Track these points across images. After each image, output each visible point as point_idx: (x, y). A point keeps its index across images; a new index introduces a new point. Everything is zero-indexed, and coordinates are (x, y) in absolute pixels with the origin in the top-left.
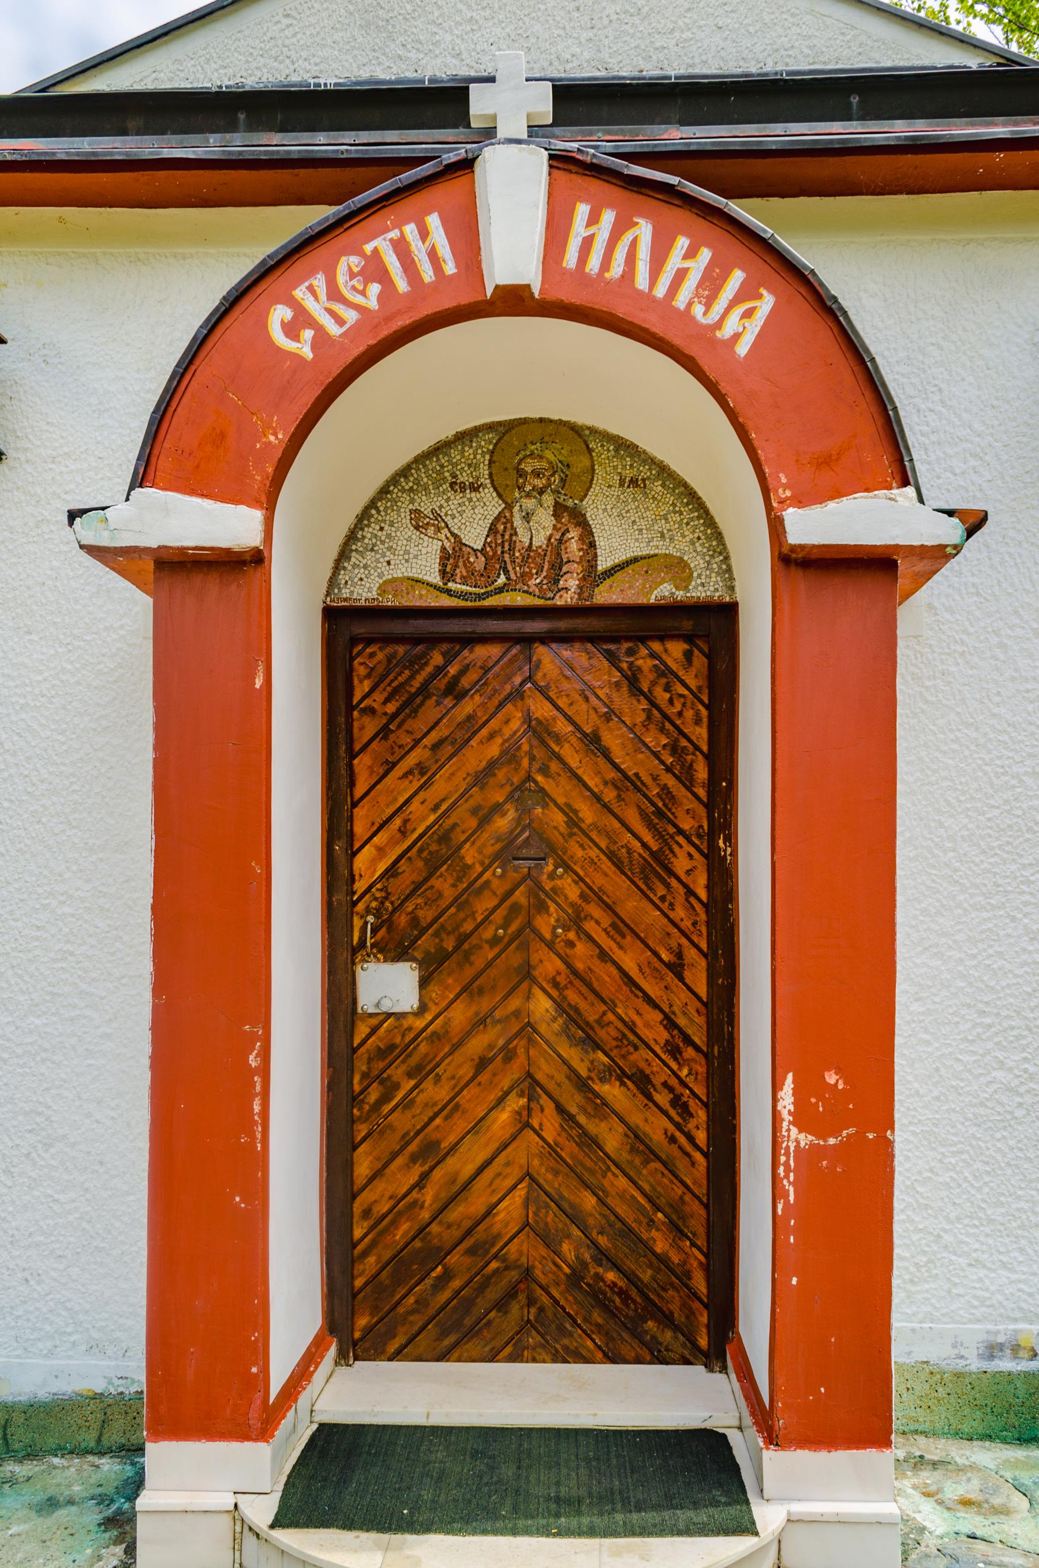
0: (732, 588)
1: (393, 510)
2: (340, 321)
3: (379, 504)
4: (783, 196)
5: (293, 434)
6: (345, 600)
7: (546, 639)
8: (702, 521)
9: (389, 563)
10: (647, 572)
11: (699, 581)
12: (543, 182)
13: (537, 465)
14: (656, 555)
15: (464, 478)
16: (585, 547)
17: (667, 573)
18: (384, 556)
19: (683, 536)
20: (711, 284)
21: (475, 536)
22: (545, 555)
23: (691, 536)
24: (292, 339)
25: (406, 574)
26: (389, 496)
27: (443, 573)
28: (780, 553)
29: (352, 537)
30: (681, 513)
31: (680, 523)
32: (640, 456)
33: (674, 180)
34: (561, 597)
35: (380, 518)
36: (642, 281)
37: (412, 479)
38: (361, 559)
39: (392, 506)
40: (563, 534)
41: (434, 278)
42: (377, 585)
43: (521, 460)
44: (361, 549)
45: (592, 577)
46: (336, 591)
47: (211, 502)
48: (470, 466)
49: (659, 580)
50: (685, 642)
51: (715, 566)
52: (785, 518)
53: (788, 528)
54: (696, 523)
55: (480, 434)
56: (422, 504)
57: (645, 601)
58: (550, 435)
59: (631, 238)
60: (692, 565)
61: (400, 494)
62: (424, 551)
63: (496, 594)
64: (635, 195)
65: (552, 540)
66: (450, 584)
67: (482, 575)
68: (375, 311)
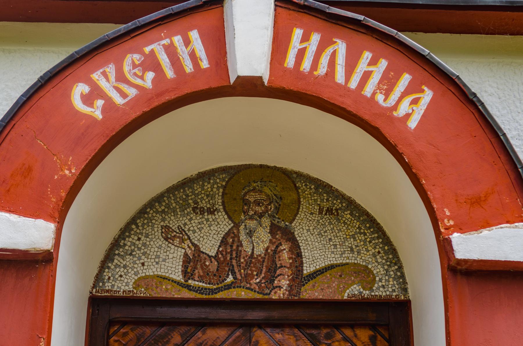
0: (405, 290)
1: (148, 226)
2: (124, 95)
3: (138, 221)
4: (426, 32)
5: (83, 170)
6: (108, 291)
7: (262, 325)
8: (381, 240)
9: (143, 264)
10: (341, 276)
11: (380, 284)
12: (271, 14)
13: (258, 197)
14: (347, 264)
15: (203, 204)
16: (294, 256)
17: (356, 277)
18: (139, 259)
19: (368, 251)
20: (388, 83)
21: (210, 246)
22: (264, 261)
23: (373, 251)
24: (88, 106)
25: (156, 273)
26: (146, 216)
27: (185, 273)
28: (449, 265)
29: (116, 244)
30: (365, 234)
31: (365, 241)
32: (333, 193)
33: (361, 17)
34: (275, 293)
35: (138, 231)
36: (340, 77)
37: (164, 204)
38: (122, 261)
39: (148, 223)
40: (277, 247)
41: (193, 70)
42: (133, 281)
43: (246, 194)
44: (122, 253)
45: (299, 278)
46: (101, 284)
47: (16, 216)
48: (208, 196)
49: (350, 282)
50: (370, 329)
51: (392, 273)
52: (453, 240)
53: (455, 247)
54: (377, 241)
55: (216, 174)
56: (171, 222)
57: (340, 298)
58: (268, 177)
59: (332, 51)
60: (375, 272)
61: (154, 215)
62: (171, 256)
63: (225, 289)
64: (334, 25)
65: (269, 251)
66: (190, 281)
67: (215, 275)
68: (150, 89)
